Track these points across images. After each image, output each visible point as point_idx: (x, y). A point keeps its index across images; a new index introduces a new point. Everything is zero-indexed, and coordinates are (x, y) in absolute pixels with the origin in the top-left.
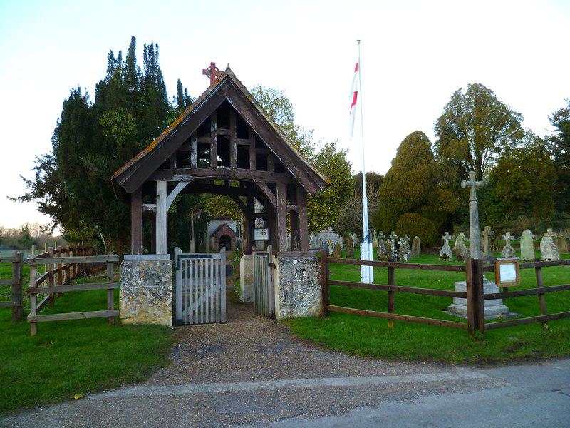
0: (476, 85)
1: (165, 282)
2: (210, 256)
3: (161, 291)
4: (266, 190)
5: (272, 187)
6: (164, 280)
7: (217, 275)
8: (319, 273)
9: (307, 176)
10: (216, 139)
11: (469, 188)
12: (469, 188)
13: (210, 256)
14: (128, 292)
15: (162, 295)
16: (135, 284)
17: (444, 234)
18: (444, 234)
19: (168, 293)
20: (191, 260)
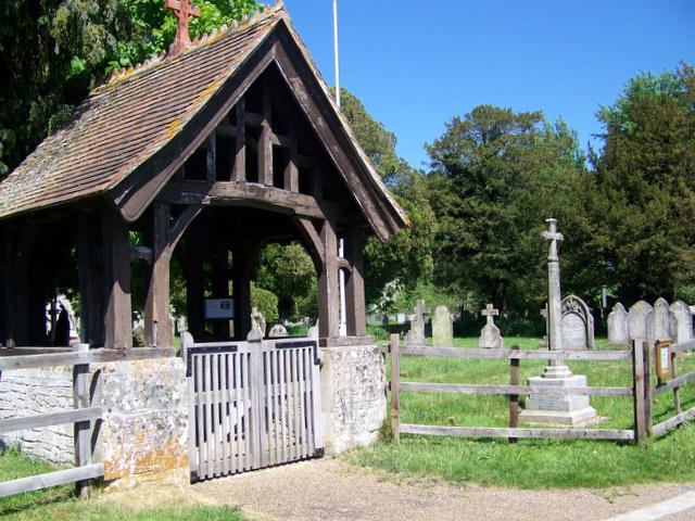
0: (475, 111)
1: (178, 401)
2: (234, 349)
3: (171, 420)
4: (308, 226)
5: (318, 224)
6: (175, 396)
7: (307, 378)
8: (382, 371)
9: (378, 208)
10: (243, 130)
11: (550, 241)
12: (550, 241)
13: (234, 349)
14: (117, 426)
15: (173, 426)
16: (128, 407)
17: (485, 308)
18: (485, 308)
19: (182, 421)
20: (282, 351)
